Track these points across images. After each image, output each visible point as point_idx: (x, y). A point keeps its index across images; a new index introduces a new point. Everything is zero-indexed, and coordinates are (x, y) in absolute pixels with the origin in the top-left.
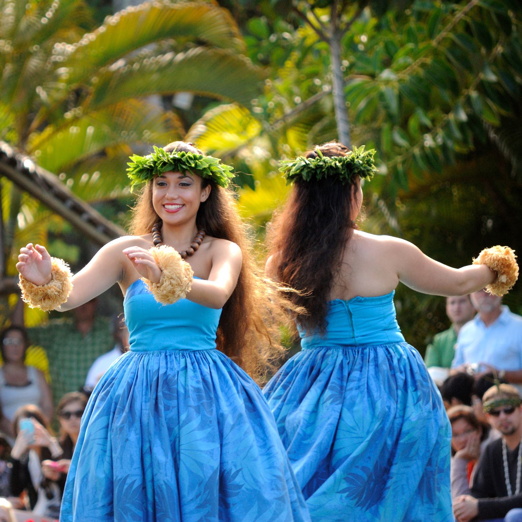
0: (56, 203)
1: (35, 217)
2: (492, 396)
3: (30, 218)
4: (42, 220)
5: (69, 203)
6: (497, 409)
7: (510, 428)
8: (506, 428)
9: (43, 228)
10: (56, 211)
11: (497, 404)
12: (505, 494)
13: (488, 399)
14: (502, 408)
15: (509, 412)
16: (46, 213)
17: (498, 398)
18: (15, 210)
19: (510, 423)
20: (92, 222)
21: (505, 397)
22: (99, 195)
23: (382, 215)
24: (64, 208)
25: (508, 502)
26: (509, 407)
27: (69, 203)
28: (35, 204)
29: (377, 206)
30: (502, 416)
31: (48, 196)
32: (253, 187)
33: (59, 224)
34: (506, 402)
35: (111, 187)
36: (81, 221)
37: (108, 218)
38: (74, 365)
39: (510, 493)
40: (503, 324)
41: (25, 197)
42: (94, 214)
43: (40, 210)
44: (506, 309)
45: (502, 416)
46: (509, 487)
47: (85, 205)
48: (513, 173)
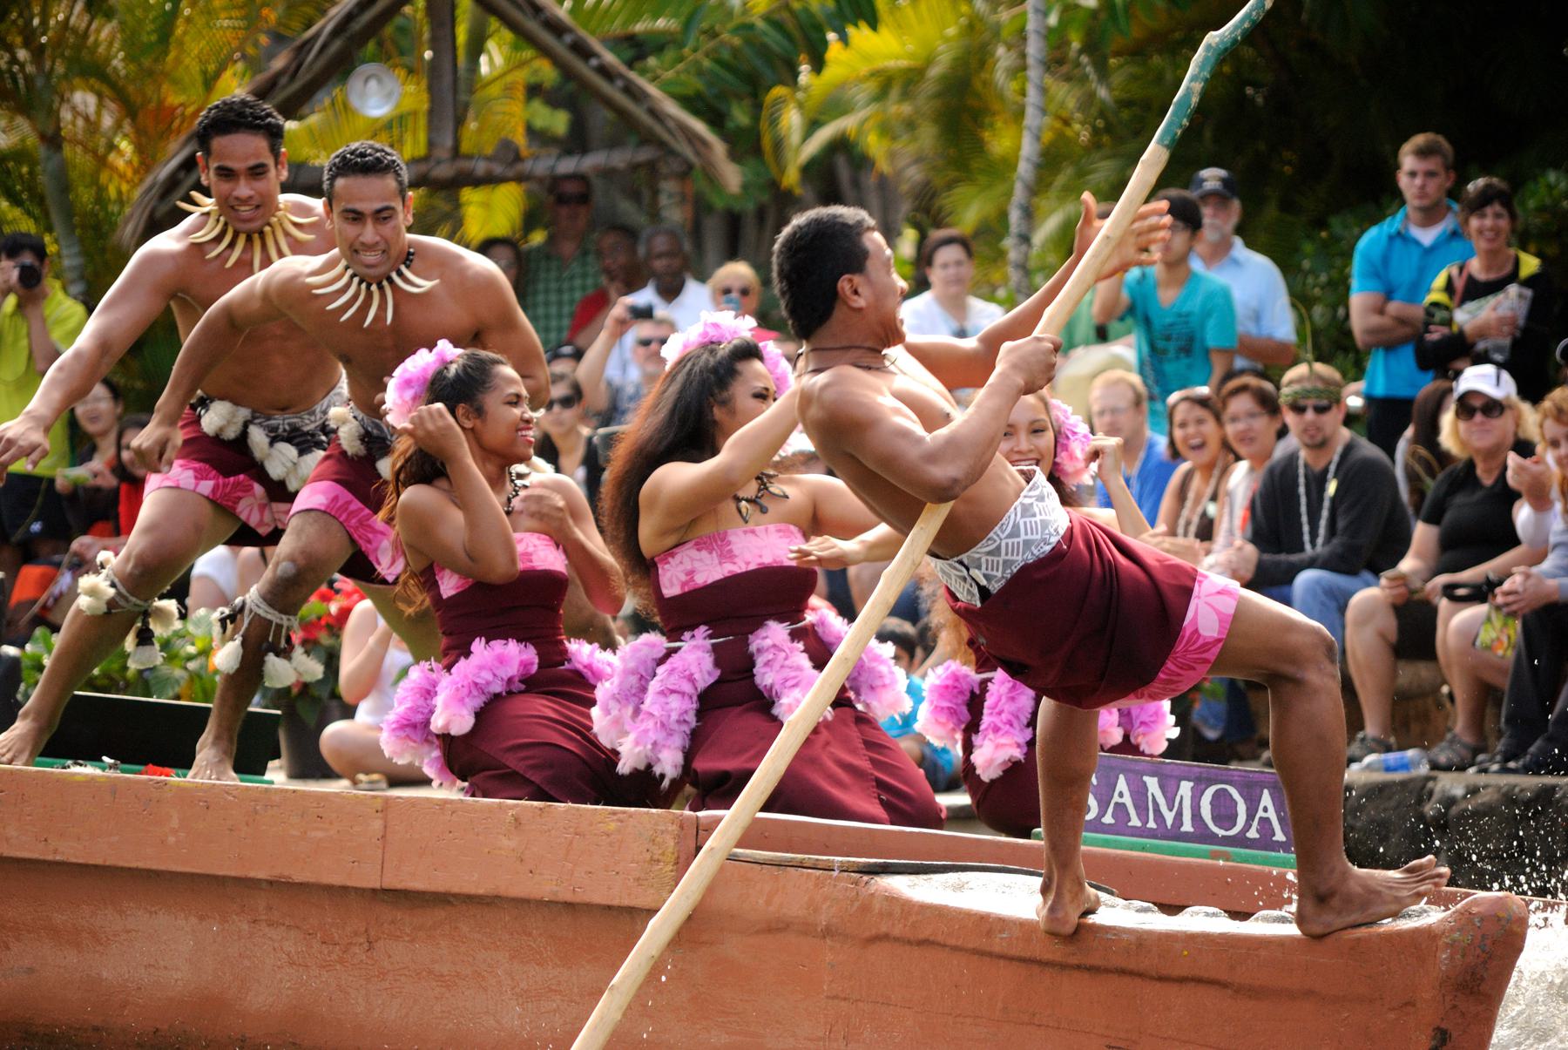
0: (547, 38)
1: (508, 60)
2: (1299, 380)
3: (499, 60)
4: (521, 65)
5: (568, 38)
6: (1302, 402)
7: (1319, 438)
8: (1312, 437)
9: (522, 76)
10: (545, 51)
11: (1306, 394)
12: (1302, 549)
13: (1291, 383)
14: (1310, 402)
15: (1320, 410)
16: (528, 53)
17: (1308, 386)
18: (477, 46)
19: (1319, 429)
20: (605, 72)
21: (1320, 386)
22: (616, 27)
23: (1084, 79)
24: (559, 48)
25: (1302, 561)
26: (1324, 402)
27: (568, 38)
28: (508, 35)
29: (1078, 65)
30: (1310, 415)
31: (532, 25)
32: (874, 24)
33: (547, 72)
34: (1319, 393)
35: (636, 16)
36: (585, 70)
37: (630, 65)
38: (553, 310)
39: (1308, 546)
40: (1236, 262)
41: (494, 23)
42: (610, 58)
43: (516, 48)
44: (1238, 242)
45: (1310, 415)
46: (1306, 538)
47: (597, 46)
48: (1304, 17)
